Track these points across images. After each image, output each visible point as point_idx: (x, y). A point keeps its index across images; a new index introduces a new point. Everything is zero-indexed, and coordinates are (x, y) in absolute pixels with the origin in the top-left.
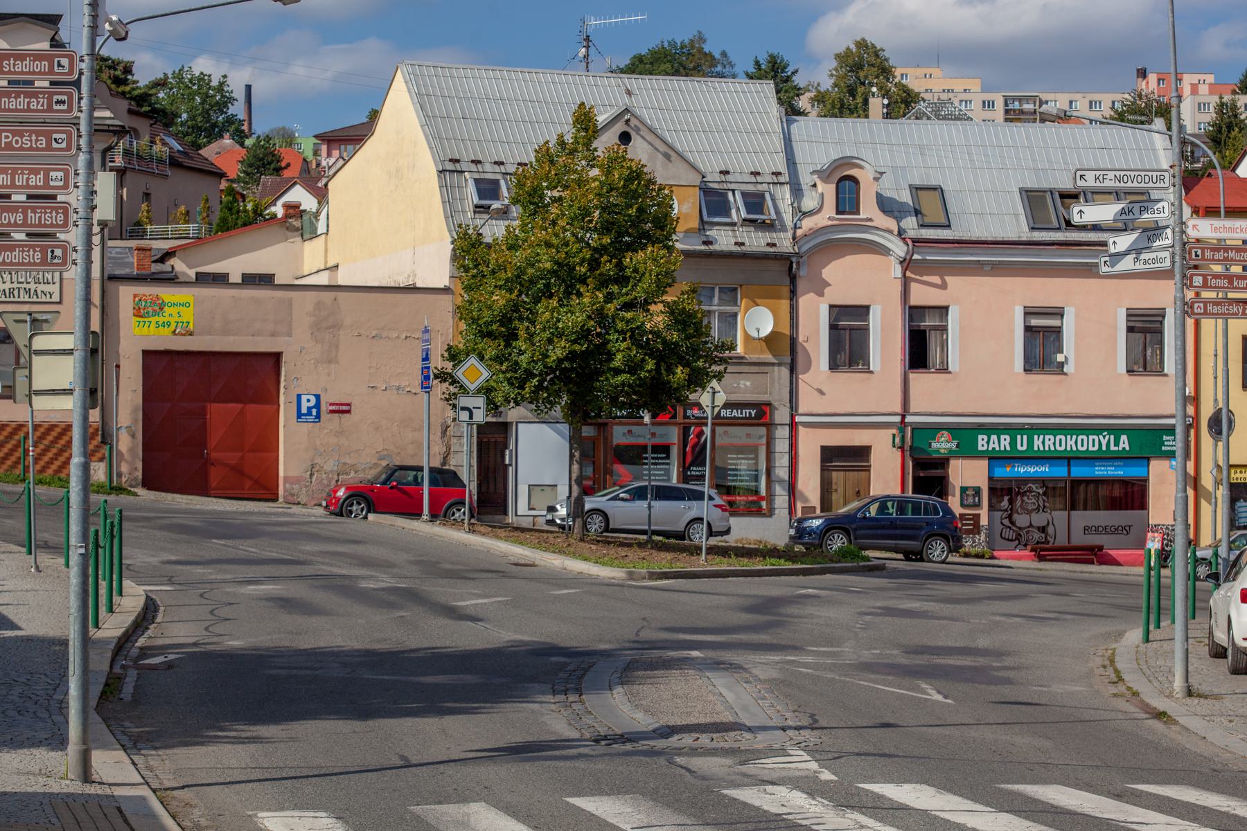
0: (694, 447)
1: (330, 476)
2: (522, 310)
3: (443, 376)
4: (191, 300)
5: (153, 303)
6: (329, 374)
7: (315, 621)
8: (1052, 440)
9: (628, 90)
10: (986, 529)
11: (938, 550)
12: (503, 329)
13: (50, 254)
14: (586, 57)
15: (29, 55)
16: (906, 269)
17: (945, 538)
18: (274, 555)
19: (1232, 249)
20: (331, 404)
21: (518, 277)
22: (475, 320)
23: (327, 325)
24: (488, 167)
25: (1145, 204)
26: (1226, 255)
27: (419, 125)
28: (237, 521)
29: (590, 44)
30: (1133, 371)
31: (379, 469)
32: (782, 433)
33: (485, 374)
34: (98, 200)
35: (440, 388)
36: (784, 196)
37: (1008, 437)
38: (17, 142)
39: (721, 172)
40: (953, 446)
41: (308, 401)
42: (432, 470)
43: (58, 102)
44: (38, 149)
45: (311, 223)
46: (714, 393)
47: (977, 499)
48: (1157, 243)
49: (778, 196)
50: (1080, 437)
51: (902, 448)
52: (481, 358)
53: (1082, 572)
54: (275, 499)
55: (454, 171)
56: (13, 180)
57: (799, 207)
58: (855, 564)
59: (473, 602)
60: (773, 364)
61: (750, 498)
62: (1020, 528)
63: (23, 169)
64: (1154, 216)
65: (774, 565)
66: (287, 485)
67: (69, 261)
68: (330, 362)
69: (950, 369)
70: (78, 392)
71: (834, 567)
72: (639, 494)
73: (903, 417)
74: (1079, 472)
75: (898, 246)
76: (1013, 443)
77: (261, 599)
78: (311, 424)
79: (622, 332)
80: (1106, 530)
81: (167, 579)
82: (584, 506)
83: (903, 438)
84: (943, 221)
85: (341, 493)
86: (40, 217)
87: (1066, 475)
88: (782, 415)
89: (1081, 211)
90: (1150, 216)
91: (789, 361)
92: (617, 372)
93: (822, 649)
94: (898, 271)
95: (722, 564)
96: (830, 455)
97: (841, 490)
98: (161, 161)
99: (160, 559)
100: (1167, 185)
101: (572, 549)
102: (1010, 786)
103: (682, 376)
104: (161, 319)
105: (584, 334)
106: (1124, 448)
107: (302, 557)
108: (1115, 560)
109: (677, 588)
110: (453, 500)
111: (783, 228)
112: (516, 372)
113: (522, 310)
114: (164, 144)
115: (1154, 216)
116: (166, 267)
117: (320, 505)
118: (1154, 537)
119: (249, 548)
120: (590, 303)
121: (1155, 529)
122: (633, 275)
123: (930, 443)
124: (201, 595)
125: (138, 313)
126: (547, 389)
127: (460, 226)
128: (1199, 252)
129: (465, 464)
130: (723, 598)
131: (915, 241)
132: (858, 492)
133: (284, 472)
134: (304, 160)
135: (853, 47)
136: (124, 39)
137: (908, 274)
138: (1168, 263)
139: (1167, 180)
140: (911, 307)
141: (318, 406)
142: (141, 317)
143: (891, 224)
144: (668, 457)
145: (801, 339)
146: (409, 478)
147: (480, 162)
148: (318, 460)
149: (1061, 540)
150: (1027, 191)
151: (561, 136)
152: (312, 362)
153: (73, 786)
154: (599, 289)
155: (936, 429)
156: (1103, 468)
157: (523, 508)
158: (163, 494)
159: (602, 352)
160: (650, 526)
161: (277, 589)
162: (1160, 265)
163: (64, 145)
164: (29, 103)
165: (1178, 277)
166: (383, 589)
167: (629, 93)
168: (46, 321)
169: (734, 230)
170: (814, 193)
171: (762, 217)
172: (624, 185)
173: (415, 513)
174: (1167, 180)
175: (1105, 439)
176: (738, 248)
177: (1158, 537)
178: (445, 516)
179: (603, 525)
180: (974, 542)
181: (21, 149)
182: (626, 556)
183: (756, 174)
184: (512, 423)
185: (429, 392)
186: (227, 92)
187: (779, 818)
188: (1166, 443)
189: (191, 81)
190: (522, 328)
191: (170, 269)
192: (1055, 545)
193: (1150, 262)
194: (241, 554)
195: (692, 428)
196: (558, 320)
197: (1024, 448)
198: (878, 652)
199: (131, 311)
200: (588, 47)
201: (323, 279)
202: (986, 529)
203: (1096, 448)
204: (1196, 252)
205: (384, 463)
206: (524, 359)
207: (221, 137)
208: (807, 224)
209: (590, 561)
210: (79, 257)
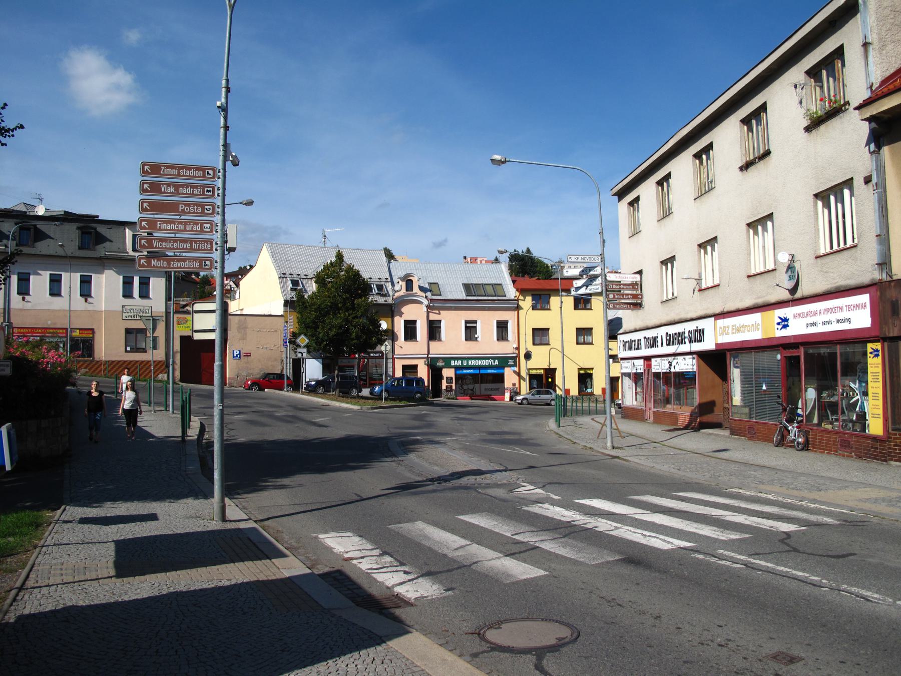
7: (267, 429)
13: (203, 264)
14: (325, 241)
15: (193, 168)
17: (356, 388)
18: (238, 404)
24: (295, 276)
32: (390, 361)
33: (307, 341)
34: (229, 238)
36: (389, 285)
38: (187, 209)
43: (208, 191)
44: (197, 213)
49: (387, 286)
51: (428, 365)
52: (305, 335)
56: (185, 227)
63: (190, 222)
67: (213, 267)
70: (218, 331)
74: (482, 371)
76: (462, 363)
80: (491, 390)
83: (428, 362)
85: (249, 383)
86: (199, 246)
92: (353, 339)
94: (425, 309)
102: (632, 497)
104: (186, 325)
105: (341, 327)
107: (249, 405)
111: (389, 296)
117: (242, 387)
121: (507, 389)
129: (288, 372)
131: (431, 300)
136: (237, 165)
141: (240, 354)
143: (423, 294)
148: (240, 372)
153: (216, 525)
163: (210, 212)
164: (193, 191)
165: (604, 295)
166: (285, 416)
168: (158, 319)
175: (490, 361)
177: (509, 391)
181: (189, 212)
183: (380, 279)
187: (569, 524)
201: (239, 312)
205: (262, 372)
206: (321, 335)
208: (397, 295)
210: (218, 265)
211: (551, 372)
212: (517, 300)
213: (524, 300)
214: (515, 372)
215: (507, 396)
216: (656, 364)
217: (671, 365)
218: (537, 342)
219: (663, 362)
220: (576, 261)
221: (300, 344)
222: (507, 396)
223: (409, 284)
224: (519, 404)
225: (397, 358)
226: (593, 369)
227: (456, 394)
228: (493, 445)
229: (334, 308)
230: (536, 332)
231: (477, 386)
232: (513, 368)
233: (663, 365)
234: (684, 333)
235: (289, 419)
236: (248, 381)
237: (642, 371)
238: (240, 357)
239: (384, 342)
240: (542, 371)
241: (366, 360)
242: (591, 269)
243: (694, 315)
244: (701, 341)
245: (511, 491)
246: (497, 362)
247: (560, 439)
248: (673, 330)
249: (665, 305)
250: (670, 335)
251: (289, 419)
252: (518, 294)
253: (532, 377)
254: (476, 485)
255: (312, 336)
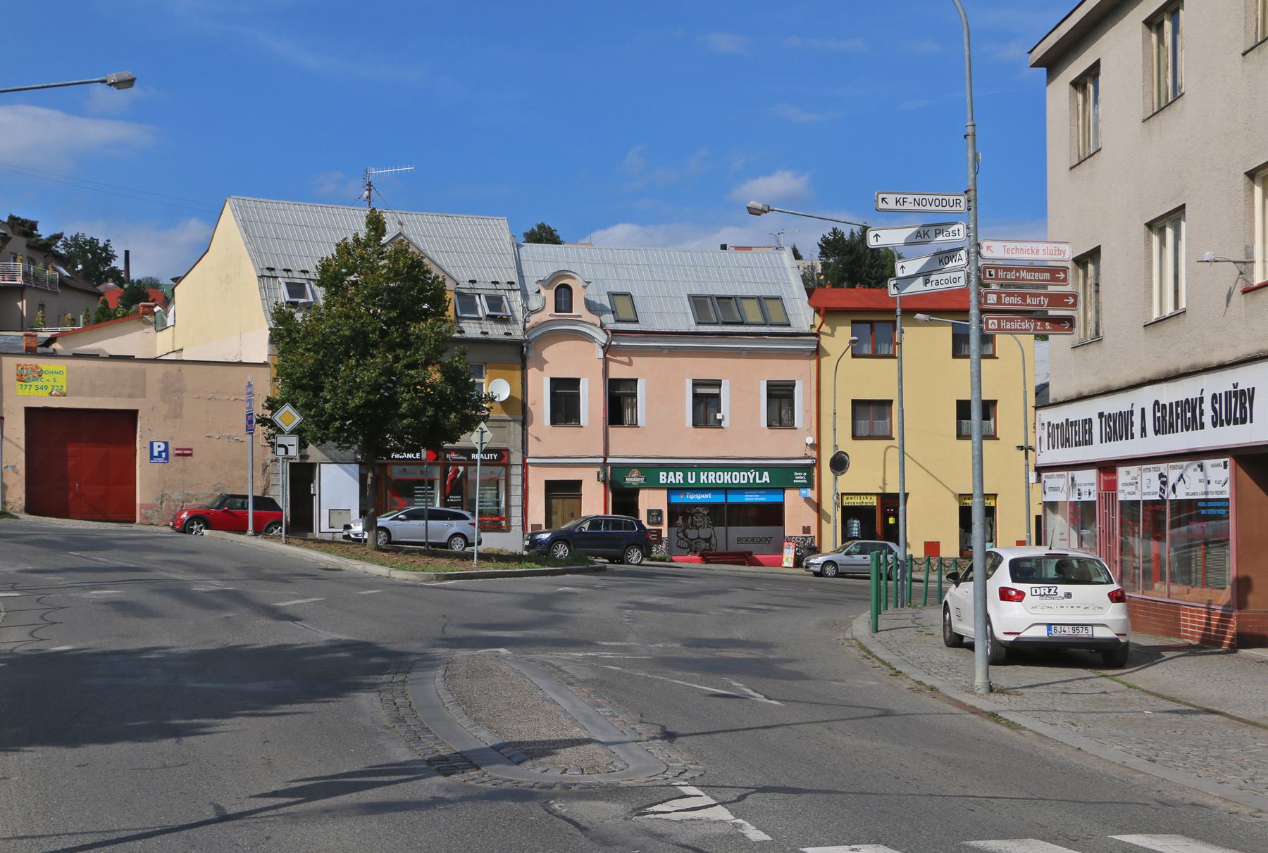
0: (451, 482)
1: (177, 503)
2: (327, 368)
3: (263, 421)
4: (64, 369)
5: (33, 370)
6: (175, 427)
8: (714, 476)
9: (400, 221)
10: (666, 540)
11: (635, 556)
12: (312, 383)
14: (369, 197)
16: (606, 353)
17: (640, 547)
19: (1023, 269)
20: (177, 449)
21: (324, 342)
22: (289, 375)
23: (172, 391)
24: (296, 274)
25: (940, 228)
26: (1018, 274)
27: (243, 243)
28: (95, 537)
29: (372, 188)
30: (771, 426)
31: (214, 498)
32: (516, 471)
33: (297, 419)
35: (260, 430)
37: (681, 474)
39: (470, 281)
40: (642, 480)
41: (159, 446)
42: (255, 498)
45: (162, 318)
46: (482, 433)
47: (659, 518)
48: (950, 264)
50: (734, 474)
51: (604, 482)
52: (294, 406)
53: (739, 571)
54: (133, 521)
55: (269, 277)
57: (527, 307)
58: (585, 567)
59: (292, 602)
60: (510, 421)
61: (494, 519)
62: (692, 540)
64: (949, 238)
65: (528, 568)
66: (143, 511)
68: (176, 417)
69: (639, 425)
71: (571, 569)
72: (412, 516)
73: (605, 459)
74: (733, 498)
75: (600, 335)
76: (685, 478)
77: (101, 603)
78: (161, 465)
79: (407, 385)
81: (9, 585)
82: (377, 523)
83: (606, 474)
84: (633, 317)
85: (184, 516)
87: (724, 501)
88: (516, 458)
89: (877, 235)
90: (946, 238)
91: (522, 419)
92: (403, 416)
93: (614, 644)
94: (600, 354)
95: (490, 568)
96: (553, 488)
97: (560, 513)
98: (52, 282)
99: (17, 569)
100: (963, 208)
101: (370, 557)
102: (981, 843)
103: (455, 420)
104: (40, 384)
105: (376, 388)
106: (766, 481)
107: (145, 565)
108: (759, 561)
109: (461, 588)
110: (271, 521)
111: (515, 322)
112: (322, 416)
113: (327, 368)
114: (55, 270)
115: (949, 238)
116: (50, 349)
117: (169, 525)
118: (789, 545)
119: (101, 558)
120: (382, 362)
121: (790, 539)
122: (416, 341)
123: (625, 478)
124: (38, 600)
125: (21, 378)
126: (347, 431)
127: (276, 303)
128: (993, 272)
129: (281, 496)
130: (501, 596)
131: (613, 332)
132: (573, 514)
133: (141, 500)
134: (166, 297)
135: (536, 228)
137: (607, 356)
138: (962, 282)
139: (963, 204)
140: (612, 381)
141: (166, 450)
142: (24, 381)
143: (595, 319)
144: (433, 489)
145: (529, 402)
146: (238, 505)
147: (290, 270)
149: (721, 548)
150: (693, 297)
151: (357, 235)
152: (162, 417)
154: (388, 352)
155: (628, 468)
156: (750, 496)
157: (325, 526)
158: (42, 518)
159: (393, 403)
160: (427, 539)
161: (117, 594)
162: (953, 285)
167: (401, 224)
169: (480, 323)
170: (538, 297)
171: (501, 314)
172: (407, 272)
173: (242, 529)
174: (963, 204)
175: (752, 475)
176: (483, 336)
177: (792, 545)
178: (266, 531)
179: (386, 538)
180: (658, 549)
182: (414, 561)
183: (495, 283)
184: (316, 464)
185: (252, 434)
186: (111, 251)
188: (796, 478)
189: (84, 243)
190: (327, 382)
191: (52, 351)
192: (717, 551)
193: (943, 282)
194: (92, 564)
195: (451, 468)
196: (356, 376)
197: (694, 481)
198: (661, 645)
199: (15, 377)
200: (370, 190)
201: (172, 357)
202: (666, 540)
203: (746, 481)
204: (990, 272)
205: (218, 494)
207: (107, 281)
208: (534, 319)
209: (386, 566)
211: (891, 502)
212: (817, 335)
213: (832, 335)
214: (808, 500)
215: (788, 557)
216: (1128, 479)
217: (1164, 483)
218: (862, 431)
219: (1146, 476)
220: (899, 207)
221: (284, 426)
222: (788, 557)
223: (564, 296)
224: (817, 574)
225: (534, 465)
226: (995, 496)
227: (669, 550)
228: (679, 673)
229: (361, 344)
230: (858, 408)
231: (720, 530)
232: (803, 491)
233: (1145, 482)
234: (1201, 400)
235: (220, 600)
236: (182, 512)
237: (1093, 498)
238: (167, 458)
239: (478, 423)
240: (874, 499)
241: (461, 468)
242: (940, 228)
243: (1229, 357)
244: (1243, 421)
245: (639, 812)
246: (766, 477)
247: (866, 661)
248: (1170, 394)
249: (1154, 331)
250: (1164, 406)
251: (220, 600)
252: (818, 320)
253: (849, 513)
254: (557, 789)
255: (307, 406)
